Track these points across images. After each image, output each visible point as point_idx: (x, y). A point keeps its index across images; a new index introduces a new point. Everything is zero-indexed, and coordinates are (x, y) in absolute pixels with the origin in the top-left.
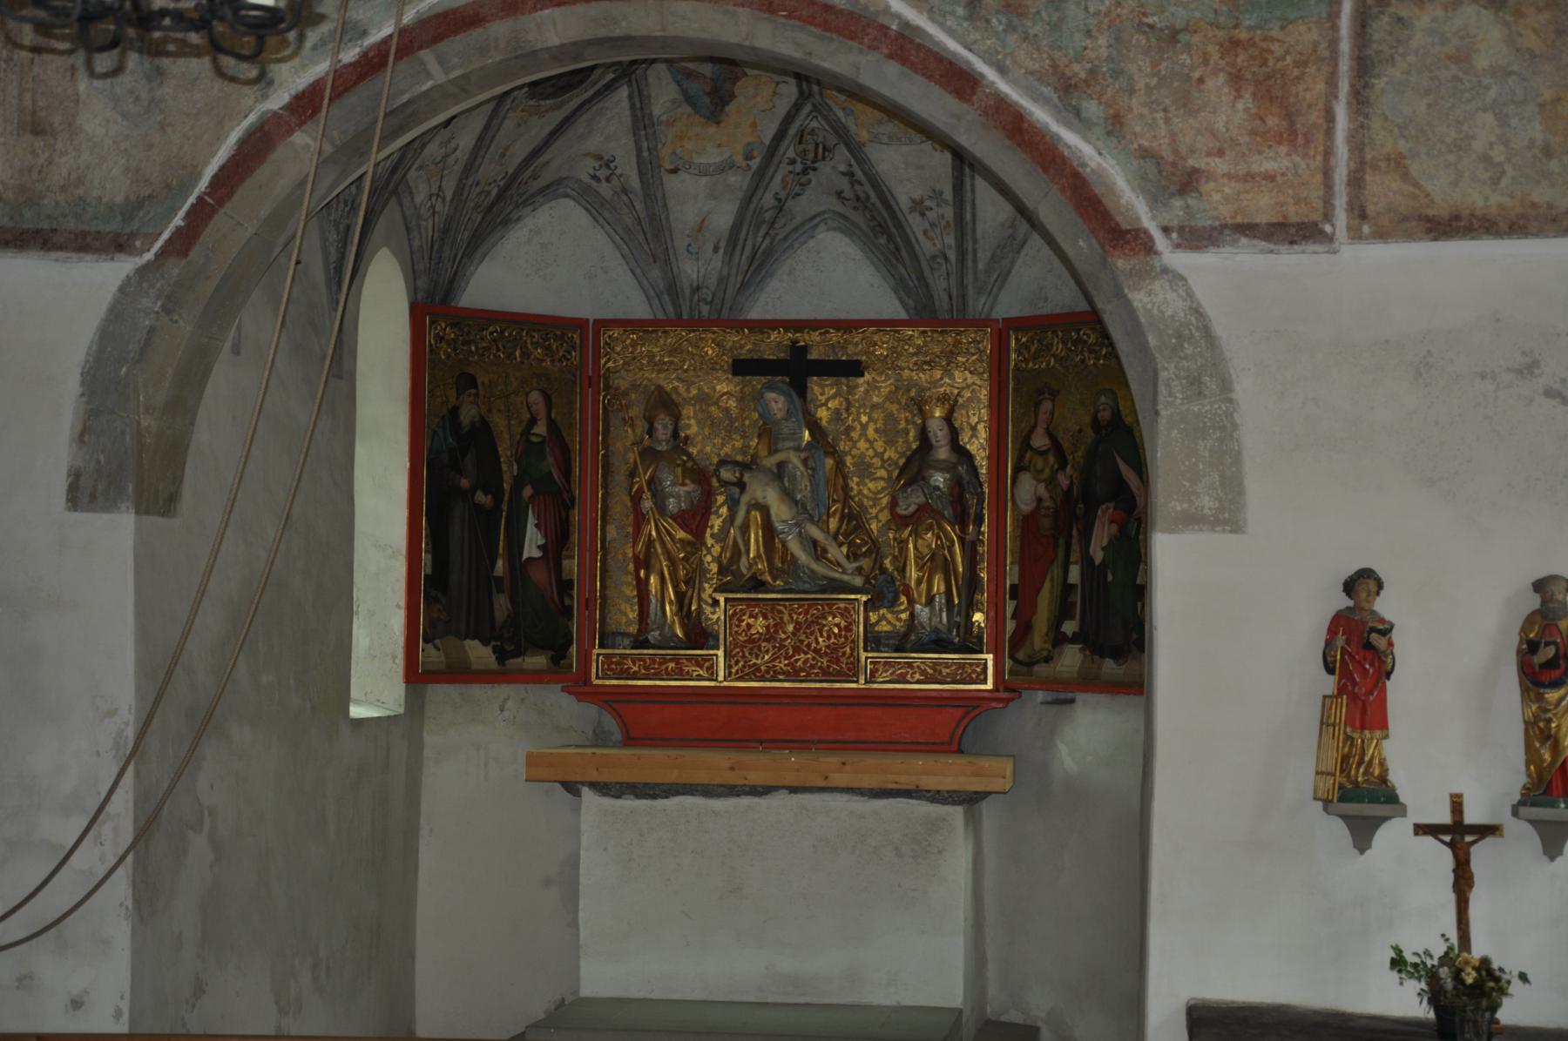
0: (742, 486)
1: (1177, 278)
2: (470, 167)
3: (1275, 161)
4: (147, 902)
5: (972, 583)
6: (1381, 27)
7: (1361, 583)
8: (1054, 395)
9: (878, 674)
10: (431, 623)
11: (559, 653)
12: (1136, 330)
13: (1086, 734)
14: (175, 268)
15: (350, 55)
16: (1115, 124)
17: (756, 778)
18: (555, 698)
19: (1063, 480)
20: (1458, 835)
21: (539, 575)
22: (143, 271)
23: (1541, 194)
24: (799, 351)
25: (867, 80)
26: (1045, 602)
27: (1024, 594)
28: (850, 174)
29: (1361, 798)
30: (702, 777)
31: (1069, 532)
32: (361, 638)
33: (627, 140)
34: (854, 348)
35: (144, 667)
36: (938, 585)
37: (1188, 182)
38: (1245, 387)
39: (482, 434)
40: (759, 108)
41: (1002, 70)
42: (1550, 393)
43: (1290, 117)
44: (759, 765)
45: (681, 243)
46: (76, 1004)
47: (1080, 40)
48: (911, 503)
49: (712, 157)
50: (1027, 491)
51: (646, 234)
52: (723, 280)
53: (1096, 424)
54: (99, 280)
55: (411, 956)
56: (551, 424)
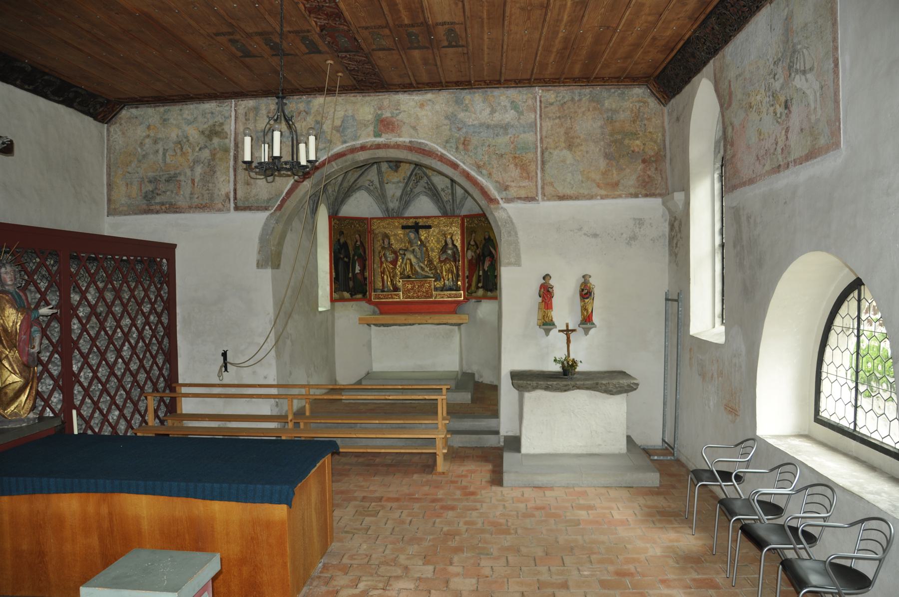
1: (505, 210)
2: (341, 185)
3: (525, 183)
4: (278, 356)
5: (458, 275)
6: (546, 154)
7: (546, 277)
9: (437, 296)
10: (336, 288)
11: (364, 294)
12: (496, 221)
13: (485, 308)
14: (278, 213)
16: (490, 175)
17: (410, 322)
18: (364, 304)
20: (568, 332)
21: (359, 277)
23: (582, 191)
24: (417, 223)
25: (433, 166)
26: (474, 279)
27: (470, 277)
29: (547, 324)
30: (398, 322)
31: (480, 263)
32: (320, 293)
33: (376, 177)
34: (430, 222)
35: (275, 304)
36: (450, 276)
37: (506, 188)
38: (520, 234)
39: (345, 243)
40: (406, 170)
41: (464, 163)
42: (585, 234)
44: (411, 318)
45: (389, 199)
46: (265, 378)
47: (481, 157)
48: (443, 257)
49: (396, 180)
50: (470, 254)
51: (381, 198)
52: (399, 208)
54: (262, 216)
55: (335, 364)
56: (361, 242)
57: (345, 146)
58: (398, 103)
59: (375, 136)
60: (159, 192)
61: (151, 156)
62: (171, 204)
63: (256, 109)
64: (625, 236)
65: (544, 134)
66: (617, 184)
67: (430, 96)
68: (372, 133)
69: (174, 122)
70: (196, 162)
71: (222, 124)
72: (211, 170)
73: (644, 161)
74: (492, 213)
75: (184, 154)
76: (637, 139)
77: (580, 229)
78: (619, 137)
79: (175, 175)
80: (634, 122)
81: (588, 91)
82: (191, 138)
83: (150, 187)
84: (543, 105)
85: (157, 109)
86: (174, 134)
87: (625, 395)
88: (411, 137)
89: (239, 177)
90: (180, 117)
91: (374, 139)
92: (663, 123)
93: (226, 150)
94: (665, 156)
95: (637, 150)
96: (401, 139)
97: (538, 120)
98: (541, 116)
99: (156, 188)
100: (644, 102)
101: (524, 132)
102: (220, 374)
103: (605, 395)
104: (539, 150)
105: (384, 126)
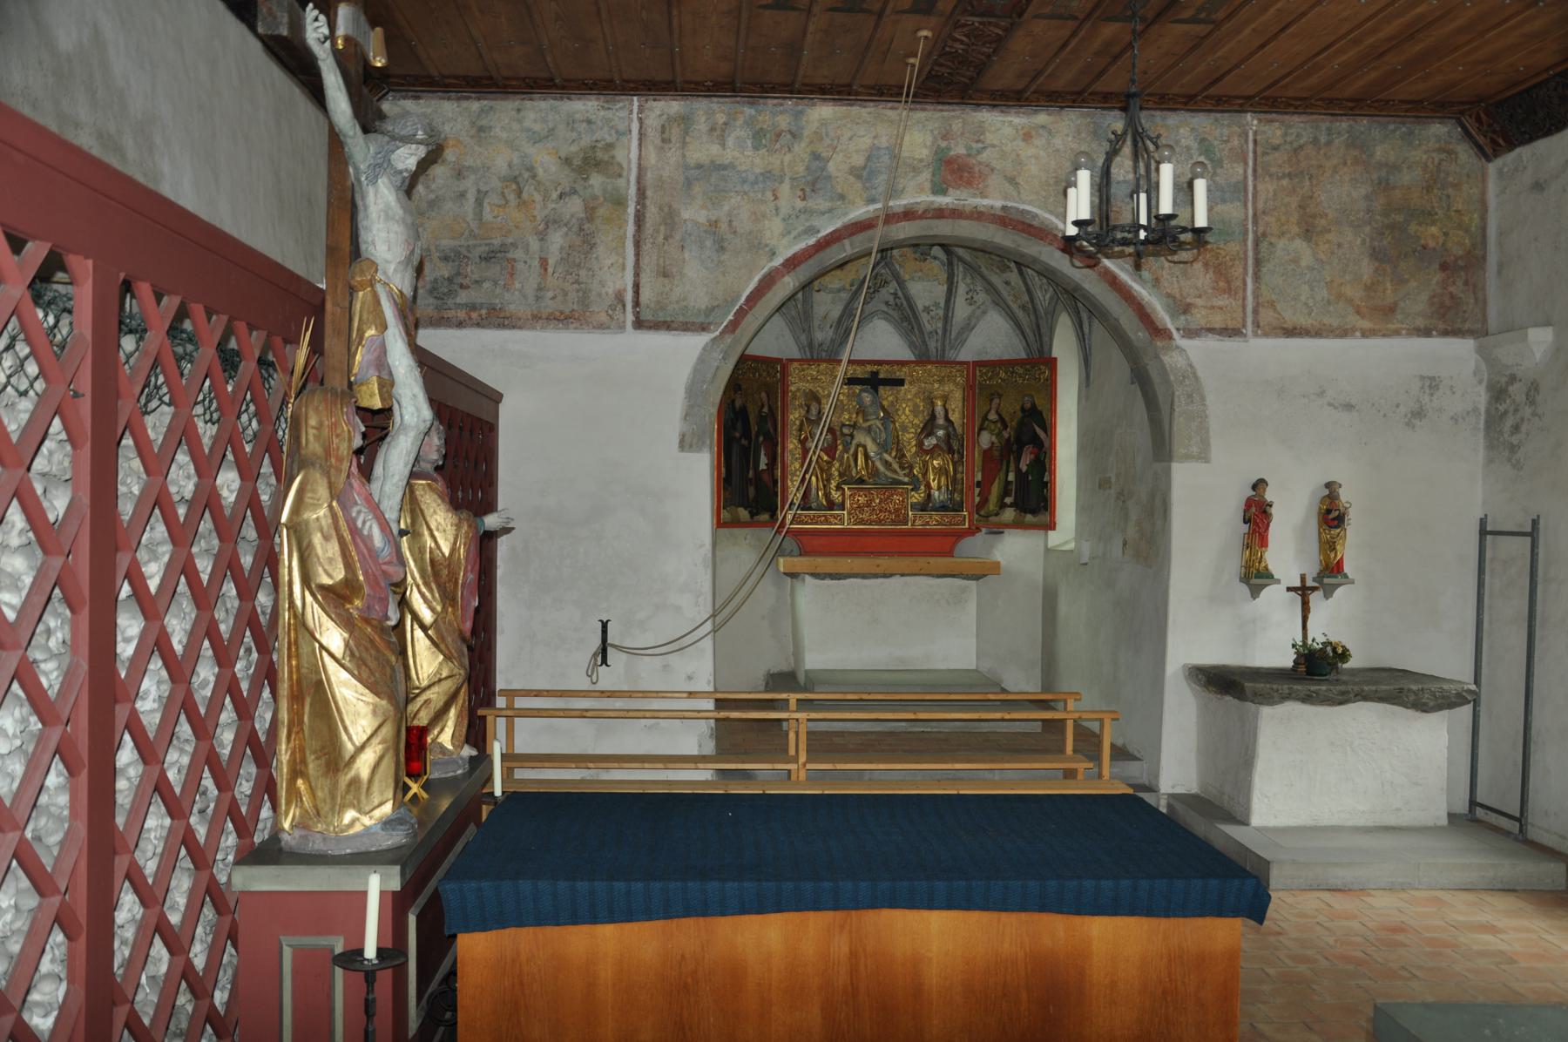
0: (852, 436)
1: (1182, 351)
3: (1221, 301)
6: (1264, 246)
7: (1259, 485)
8: (1000, 396)
12: (1164, 372)
14: (729, 339)
15: (812, 241)
16: (1156, 282)
19: (1006, 435)
21: (766, 477)
23: (1327, 320)
27: (984, 486)
28: (895, 294)
29: (1256, 577)
37: (1187, 309)
38: (1210, 399)
42: (1330, 404)
43: (1228, 282)
45: (816, 323)
46: (690, 678)
49: (836, 285)
50: (986, 439)
52: (832, 341)
53: (1023, 409)
57: (872, 207)
58: (981, 130)
59: (934, 193)
60: (466, 282)
61: (449, 205)
62: (492, 309)
63: (685, 121)
64: (1402, 409)
65: (1260, 206)
66: (1392, 309)
67: (1042, 118)
68: (928, 185)
69: (504, 135)
70: (551, 222)
71: (610, 146)
72: (585, 241)
73: (1444, 267)
74: (1157, 357)
75: (523, 204)
76: (1433, 223)
77: (1322, 394)
78: (1400, 218)
79: (504, 249)
80: (1428, 189)
81: (1344, 125)
82: (540, 171)
83: (445, 271)
84: (1260, 150)
85: (465, 104)
86: (501, 161)
87: (1445, 712)
88: (1006, 198)
89: (645, 261)
90: (515, 126)
91: (932, 198)
92: (1483, 193)
93: (620, 202)
94: (1484, 258)
95: (1431, 244)
96: (985, 202)
97: (1250, 178)
98: (1255, 171)
99: (458, 274)
100: (1450, 153)
101: (1224, 201)
103: (1411, 712)
104: (1251, 237)
105: (953, 172)
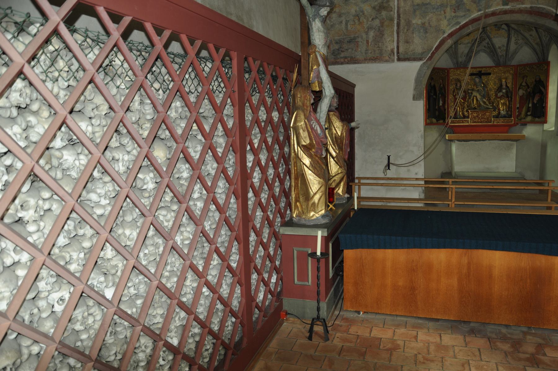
0: (472, 93)
8: (527, 77)
14: (429, 62)
15: (458, 27)
22: (424, 63)
26: (524, 110)
39: (434, 86)
46: (416, 174)
50: (521, 92)
52: (465, 61)
53: (536, 81)
54: (417, 65)
57: (479, 13)
59: (503, 5)
60: (343, 50)
62: (352, 58)
68: (501, 3)
70: (370, 28)
72: (380, 34)
75: (360, 23)
79: (355, 38)
82: (366, 12)
83: (337, 47)
89: (401, 38)
91: (502, 7)
93: (392, 20)
96: (523, 6)
99: (341, 47)
102: (384, 172)
